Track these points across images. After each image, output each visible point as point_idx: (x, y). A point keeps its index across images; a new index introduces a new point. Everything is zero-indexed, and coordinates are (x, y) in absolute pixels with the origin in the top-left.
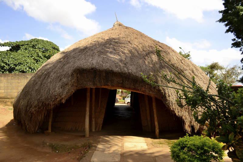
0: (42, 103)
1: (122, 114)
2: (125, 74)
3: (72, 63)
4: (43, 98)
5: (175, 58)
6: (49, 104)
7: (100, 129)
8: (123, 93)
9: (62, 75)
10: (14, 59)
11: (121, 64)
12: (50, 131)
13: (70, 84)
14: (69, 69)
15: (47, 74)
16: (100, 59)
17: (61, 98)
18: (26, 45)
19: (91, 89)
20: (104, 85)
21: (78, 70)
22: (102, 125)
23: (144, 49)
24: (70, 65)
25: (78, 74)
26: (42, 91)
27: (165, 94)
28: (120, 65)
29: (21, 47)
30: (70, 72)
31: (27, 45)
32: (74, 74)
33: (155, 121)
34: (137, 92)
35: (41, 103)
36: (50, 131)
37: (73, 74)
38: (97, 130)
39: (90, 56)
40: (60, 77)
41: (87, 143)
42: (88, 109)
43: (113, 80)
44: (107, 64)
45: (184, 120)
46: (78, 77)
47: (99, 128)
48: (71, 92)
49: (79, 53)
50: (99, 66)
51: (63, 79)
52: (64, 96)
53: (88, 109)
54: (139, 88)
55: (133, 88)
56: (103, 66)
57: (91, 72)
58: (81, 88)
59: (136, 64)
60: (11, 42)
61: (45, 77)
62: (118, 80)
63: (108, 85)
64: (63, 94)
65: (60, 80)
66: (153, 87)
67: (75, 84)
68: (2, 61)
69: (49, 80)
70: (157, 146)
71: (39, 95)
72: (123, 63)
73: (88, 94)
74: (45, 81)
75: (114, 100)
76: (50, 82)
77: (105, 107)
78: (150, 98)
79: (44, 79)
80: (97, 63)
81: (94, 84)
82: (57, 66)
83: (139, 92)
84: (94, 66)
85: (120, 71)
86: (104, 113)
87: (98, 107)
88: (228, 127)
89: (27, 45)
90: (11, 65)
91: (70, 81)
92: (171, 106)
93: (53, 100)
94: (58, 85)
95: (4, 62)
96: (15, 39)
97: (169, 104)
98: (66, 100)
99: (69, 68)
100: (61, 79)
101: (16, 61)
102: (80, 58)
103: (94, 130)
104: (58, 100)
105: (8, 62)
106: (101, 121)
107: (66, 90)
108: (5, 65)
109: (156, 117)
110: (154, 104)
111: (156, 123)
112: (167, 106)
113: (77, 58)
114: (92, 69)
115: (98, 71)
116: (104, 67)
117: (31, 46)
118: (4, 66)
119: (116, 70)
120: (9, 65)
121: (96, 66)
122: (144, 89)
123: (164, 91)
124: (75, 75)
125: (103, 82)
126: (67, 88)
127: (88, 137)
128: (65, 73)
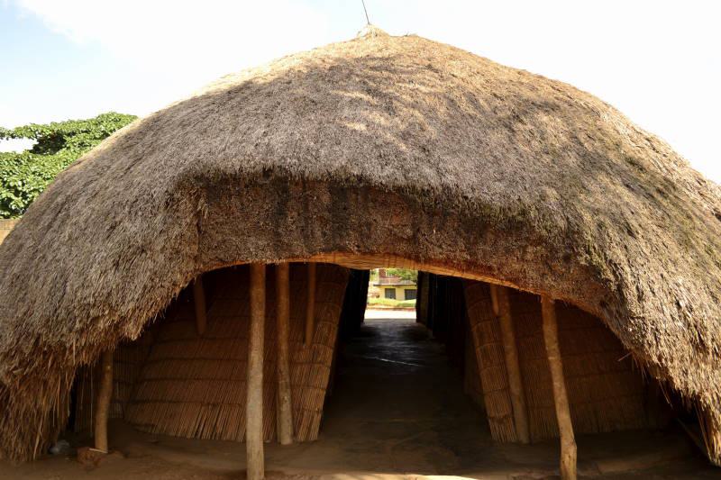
1: (393, 357)
2: (425, 193)
3: (171, 149)
4: (37, 316)
7: (314, 434)
8: (384, 277)
9: (120, 204)
10: (40, 175)
11: (403, 147)
13: (159, 248)
16: (306, 129)
18: (83, 132)
19: (271, 270)
20: (327, 251)
21: (199, 178)
23: (497, 93)
24: (160, 157)
25: (202, 201)
27: (621, 286)
28: (398, 153)
29: (68, 139)
30: (159, 192)
31: (86, 132)
33: (558, 406)
34: (479, 279)
35: (33, 341)
38: (301, 437)
42: (256, 357)
43: (369, 225)
45: (709, 407)
46: (198, 215)
51: (127, 224)
52: (131, 306)
53: (256, 357)
54: (493, 262)
57: (261, 186)
59: (473, 147)
60: (38, 126)
63: (342, 250)
64: (124, 297)
65: (113, 228)
66: (561, 255)
68: (5, 182)
72: (415, 145)
73: (258, 292)
75: (361, 303)
76: (70, 238)
77: (333, 339)
78: (524, 305)
79: (50, 226)
81: (278, 245)
83: (488, 280)
84: (274, 160)
85: (402, 181)
86: (329, 364)
87: (304, 341)
89: (86, 132)
90: (30, 196)
92: (650, 345)
93: (78, 326)
95: (9, 187)
96: (50, 116)
97: (644, 336)
98: (148, 327)
99: (158, 175)
101: (47, 183)
103: (286, 440)
104: (101, 325)
105: (23, 185)
106: (315, 399)
107: (143, 279)
108: (13, 197)
109: (563, 391)
110: (550, 331)
111: (564, 418)
112: (627, 345)
114: (267, 172)
115: (297, 184)
117: (98, 136)
118: (10, 200)
119: (380, 173)
120: (24, 196)
121: (283, 157)
122: (517, 267)
123: (614, 273)
124: (185, 205)
125: (319, 233)
126: (145, 268)
128: (136, 192)
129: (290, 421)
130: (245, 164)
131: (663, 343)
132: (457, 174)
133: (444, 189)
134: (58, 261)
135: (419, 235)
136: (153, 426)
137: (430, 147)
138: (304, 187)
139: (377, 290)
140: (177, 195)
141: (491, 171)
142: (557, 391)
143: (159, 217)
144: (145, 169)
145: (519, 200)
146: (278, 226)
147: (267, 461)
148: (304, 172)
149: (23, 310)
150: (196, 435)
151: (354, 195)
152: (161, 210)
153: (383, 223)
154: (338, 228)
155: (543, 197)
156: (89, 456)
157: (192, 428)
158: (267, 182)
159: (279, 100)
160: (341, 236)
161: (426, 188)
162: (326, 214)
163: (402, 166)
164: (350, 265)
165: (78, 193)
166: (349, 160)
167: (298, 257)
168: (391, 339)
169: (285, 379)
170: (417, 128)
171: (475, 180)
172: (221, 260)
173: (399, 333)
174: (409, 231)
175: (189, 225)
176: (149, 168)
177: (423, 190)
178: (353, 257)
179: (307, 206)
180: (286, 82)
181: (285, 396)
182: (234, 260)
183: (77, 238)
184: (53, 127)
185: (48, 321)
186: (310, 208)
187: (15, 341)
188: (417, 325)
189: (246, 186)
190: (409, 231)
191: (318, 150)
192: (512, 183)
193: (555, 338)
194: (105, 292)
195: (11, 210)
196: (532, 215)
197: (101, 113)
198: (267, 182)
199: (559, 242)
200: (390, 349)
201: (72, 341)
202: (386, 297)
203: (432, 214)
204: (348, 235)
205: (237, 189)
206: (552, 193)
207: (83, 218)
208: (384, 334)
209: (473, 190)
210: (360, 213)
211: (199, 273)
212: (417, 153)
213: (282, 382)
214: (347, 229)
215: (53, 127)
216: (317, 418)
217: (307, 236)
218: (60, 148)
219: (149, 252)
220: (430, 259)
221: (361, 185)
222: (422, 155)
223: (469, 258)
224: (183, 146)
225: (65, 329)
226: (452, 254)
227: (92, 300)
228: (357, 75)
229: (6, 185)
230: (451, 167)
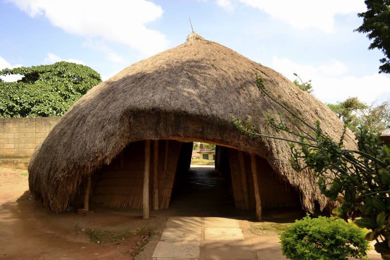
0: (75, 165)
1: (202, 182)
2: (206, 117)
3: (121, 101)
5: (287, 91)
6: (84, 166)
9: (104, 120)
10: (28, 94)
11: (199, 101)
12: (86, 208)
15: (81, 118)
16: (166, 94)
18: (48, 72)
19: (152, 142)
20: (173, 136)
21: (131, 111)
25: (132, 118)
26: (73, 145)
27: (271, 149)
28: (197, 104)
29: (41, 75)
30: (118, 115)
31: (49, 71)
33: (255, 193)
34: (226, 146)
35: (73, 165)
36: (86, 208)
38: (162, 207)
40: (102, 123)
41: (146, 229)
42: (147, 174)
44: (177, 101)
45: (302, 191)
46: (130, 123)
47: (165, 204)
49: (133, 85)
51: (108, 126)
52: (109, 153)
53: (147, 174)
54: (229, 140)
57: (152, 114)
58: (135, 140)
60: (25, 68)
63: (179, 136)
64: (106, 150)
65: (103, 127)
67: (126, 135)
68: (11, 98)
69: (85, 128)
73: (147, 150)
74: (78, 129)
78: (246, 156)
79: (77, 126)
80: (161, 99)
81: (157, 133)
82: (97, 106)
85: (198, 113)
86: (173, 179)
87: (163, 170)
89: (49, 71)
90: (24, 105)
93: (91, 159)
96: (31, 62)
97: (279, 166)
99: (116, 108)
101: (32, 98)
102: (134, 92)
103: (156, 208)
104: (99, 159)
105: (20, 99)
106: (167, 193)
107: (112, 144)
108: (15, 105)
109: (257, 187)
114: (154, 109)
118: (14, 107)
119: (192, 110)
120: (21, 105)
123: (269, 145)
124: (126, 120)
125: (170, 130)
126: (114, 140)
130: (146, 107)
131: (285, 168)
132: (217, 111)
139: (199, 155)
140: (124, 117)
142: (255, 187)
147: (150, 214)
149: (69, 154)
153: (192, 127)
155: (246, 118)
158: (153, 113)
162: (173, 123)
164: (180, 141)
165: (88, 114)
168: (201, 176)
172: (137, 139)
173: (206, 173)
174: (201, 130)
175: (127, 126)
178: (182, 138)
179: (166, 121)
180: (159, 73)
181: (156, 191)
182: (142, 138)
184: (33, 69)
185: (80, 158)
190: (201, 130)
195: (14, 112)
197: (57, 61)
198: (153, 113)
200: (200, 179)
201: (89, 165)
202: (204, 158)
204: (180, 131)
206: (250, 117)
207: (90, 124)
208: (199, 174)
213: (155, 185)
215: (33, 69)
216: (168, 200)
218: (36, 80)
227: (97, 151)
228: (185, 70)
229: (12, 99)
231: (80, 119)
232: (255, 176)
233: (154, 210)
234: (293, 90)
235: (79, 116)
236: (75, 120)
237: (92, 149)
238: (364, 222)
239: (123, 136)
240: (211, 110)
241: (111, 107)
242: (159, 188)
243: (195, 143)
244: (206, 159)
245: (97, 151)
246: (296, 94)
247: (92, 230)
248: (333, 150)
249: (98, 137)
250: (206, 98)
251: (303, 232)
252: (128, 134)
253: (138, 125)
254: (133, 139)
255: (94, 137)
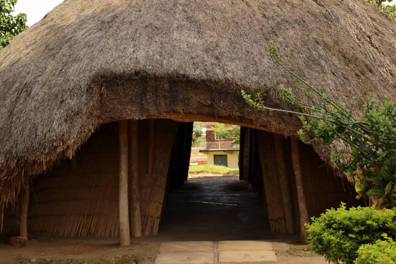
0: (18, 162)
2: (216, 83)
4: (21, 147)
5: (353, 32)
6: (35, 162)
8: (214, 140)
12: (24, 236)
14: (82, 75)
15: (22, 89)
16: (154, 48)
17: (65, 147)
20: (167, 113)
21: (103, 76)
22: (159, 221)
26: (14, 131)
30: (84, 84)
32: (93, 88)
35: (15, 161)
36: (24, 236)
37: (90, 88)
38: (147, 233)
39: (127, 39)
40: (60, 96)
41: (130, 256)
42: (124, 175)
43: (189, 99)
44: (172, 60)
46: (101, 95)
47: (152, 228)
48: (86, 130)
50: (153, 66)
51: (69, 101)
52: (73, 141)
53: (124, 175)
55: (239, 117)
56: (162, 65)
57: (134, 80)
58: (108, 121)
59: (244, 56)
61: (18, 98)
62: (201, 98)
63: (176, 112)
65: (61, 102)
67: (95, 113)
70: (300, 254)
71: (8, 140)
73: (123, 138)
74: (19, 106)
77: (166, 172)
79: (16, 101)
80: (147, 57)
81: (142, 110)
82: (46, 68)
84: (140, 66)
85: (204, 77)
86: (164, 188)
88: (383, 173)
91: (85, 104)
93: (47, 151)
94: (58, 115)
100: (63, 100)
102: (104, 46)
103: (138, 234)
106: (155, 209)
107: (77, 128)
109: (302, 191)
110: (295, 157)
113: (98, 47)
115: (152, 79)
116: (165, 66)
119: (195, 73)
121: (145, 66)
125: (163, 104)
127: (127, 246)
128: (72, 85)
129: (140, 222)
132: (233, 73)
133: (226, 81)
134: (30, 119)
135: (214, 104)
136: (46, 231)
137: (220, 57)
138: (156, 80)
139: (205, 157)
141: (251, 69)
142: (298, 191)
143: (84, 97)
144: (75, 72)
145: (265, 85)
146: (142, 100)
148: (156, 73)
150: (77, 234)
151: (181, 84)
152: (85, 93)
153: (196, 99)
154: (173, 100)
156: (18, 241)
157: (74, 230)
158: (137, 78)
159: (137, 27)
160: (175, 105)
161: (217, 80)
162: (167, 94)
163: (205, 69)
164: (179, 120)
165: (35, 82)
166: (178, 67)
167: (152, 116)
168: (212, 191)
169: (137, 195)
170: (214, 44)
171: (242, 75)
172: (112, 118)
173: (221, 187)
174: (209, 102)
175: (97, 100)
176: (76, 71)
177: (215, 81)
178: (180, 115)
179: (157, 90)
182: (119, 118)
183: (39, 108)
186: (159, 91)
187: (5, 161)
188: (239, 181)
189: (126, 80)
190: (209, 102)
191: (162, 61)
192: (263, 75)
193: (298, 161)
194: (61, 134)
196: (271, 93)
198: (137, 78)
199: (286, 106)
200: (210, 196)
201: (43, 159)
202: (216, 163)
203: (220, 93)
204: (178, 104)
205: (122, 82)
209: (241, 80)
210: (183, 93)
211: (100, 125)
212: (213, 61)
213: (134, 197)
214: (177, 101)
216: (157, 222)
217: (157, 105)
219: (80, 115)
220: (220, 116)
221: (184, 79)
222: (216, 62)
223: (240, 115)
224: (92, 59)
225: (38, 153)
226: (231, 113)
230: (230, 68)
231: (20, 91)
232: (298, 174)
233: (134, 236)
234: (364, 30)
235: (17, 85)
236: (11, 92)
237: (47, 135)
238: (374, 192)
239: (92, 114)
240: (224, 73)
241: (71, 71)
242: (141, 201)
243: (200, 127)
244: (220, 164)
245: (55, 138)
246: (369, 37)
247: (48, 260)
248: (339, 122)
249: (57, 117)
250: (217, 53)
251: (332, 221)
252: (99, 111)
253: (113, 97)
254: (106, 119)
255: (49, 117)
